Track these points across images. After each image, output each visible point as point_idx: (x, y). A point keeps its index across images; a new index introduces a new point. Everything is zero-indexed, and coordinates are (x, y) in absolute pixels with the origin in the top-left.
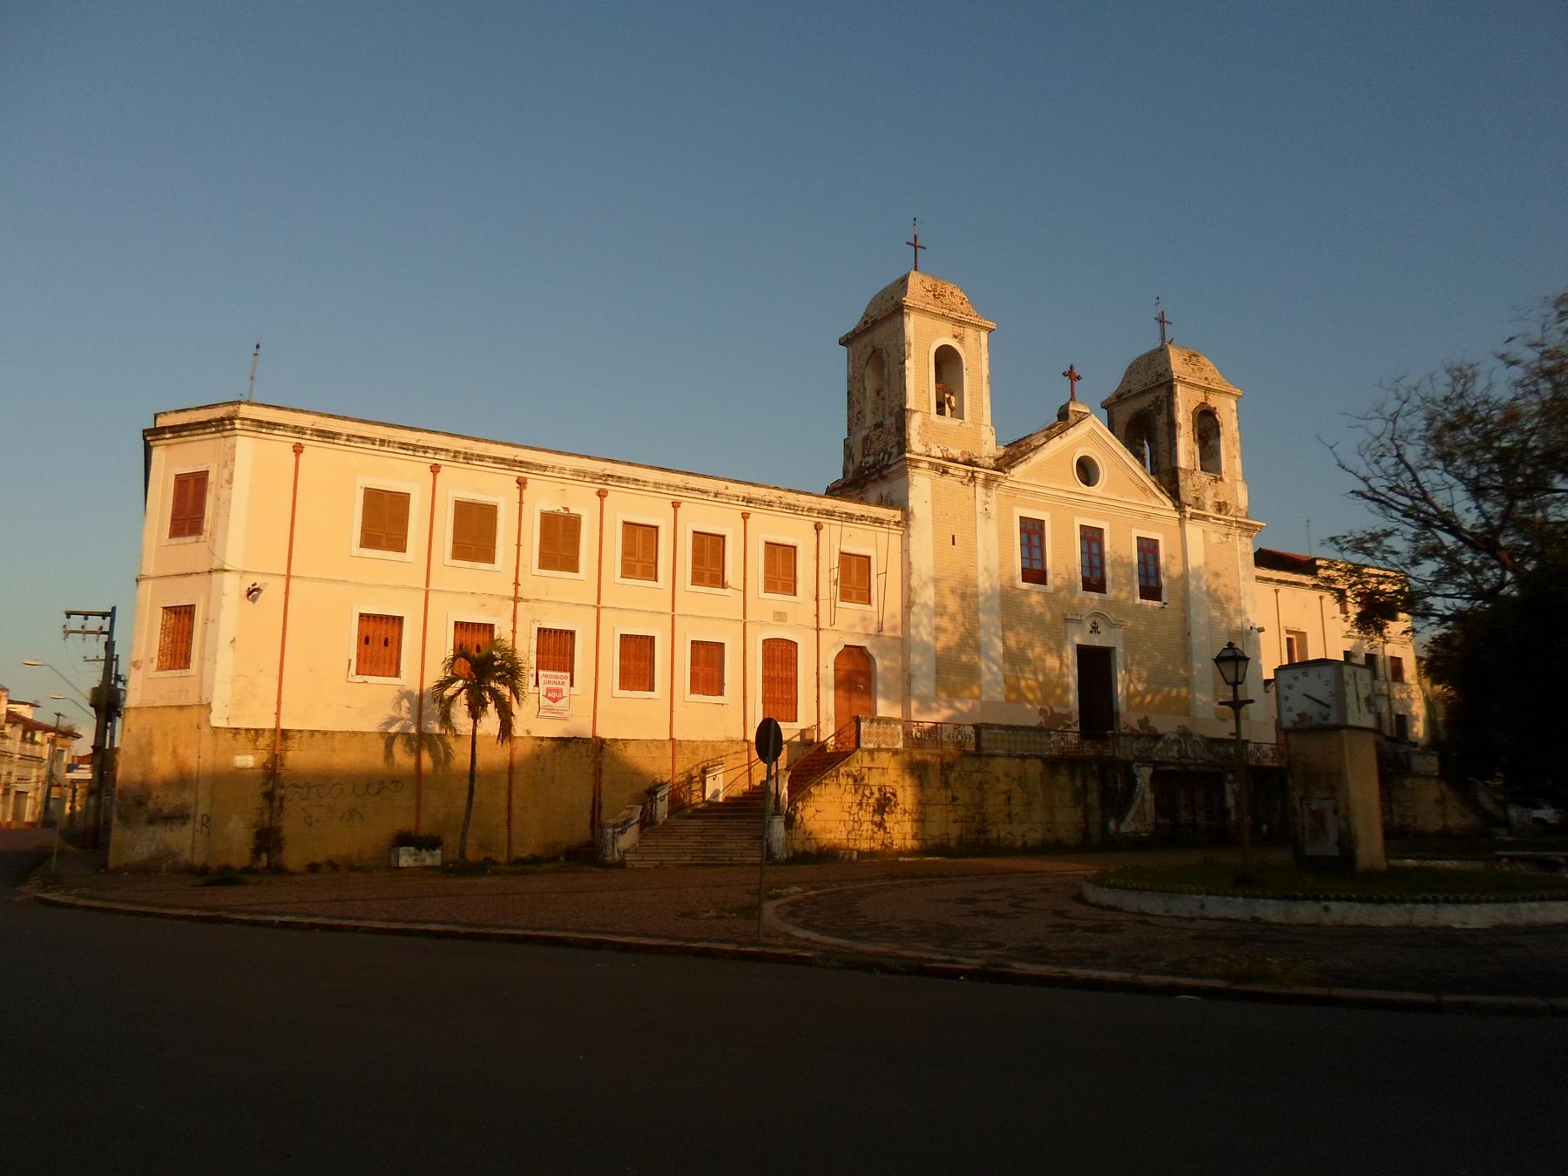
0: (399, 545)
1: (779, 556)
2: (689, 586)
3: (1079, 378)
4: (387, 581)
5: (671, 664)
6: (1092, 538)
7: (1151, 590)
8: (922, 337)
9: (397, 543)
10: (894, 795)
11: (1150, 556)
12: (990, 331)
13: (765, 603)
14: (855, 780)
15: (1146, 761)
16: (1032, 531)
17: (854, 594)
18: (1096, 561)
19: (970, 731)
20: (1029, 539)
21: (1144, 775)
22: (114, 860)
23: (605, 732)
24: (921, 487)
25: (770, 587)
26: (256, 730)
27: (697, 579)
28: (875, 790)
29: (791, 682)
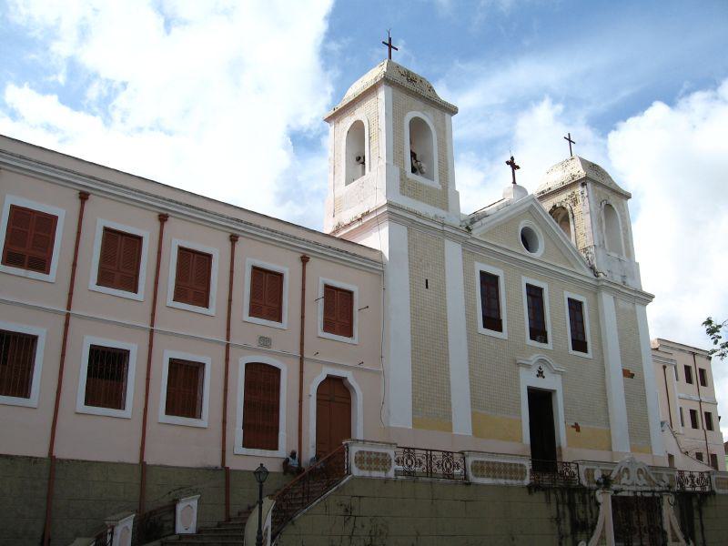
0: (42, 265)
2: (170, 302)
3: (518, 168)
5: (145, 383)
6: (535, 294)
7: (580, 344)
9: (41, 263)
13: (249, 327)
16: (489, 282)
20: (576, 325)
21: (604, 499)
22: (720, 470)
23: (60, 453)
25: (254, 311)
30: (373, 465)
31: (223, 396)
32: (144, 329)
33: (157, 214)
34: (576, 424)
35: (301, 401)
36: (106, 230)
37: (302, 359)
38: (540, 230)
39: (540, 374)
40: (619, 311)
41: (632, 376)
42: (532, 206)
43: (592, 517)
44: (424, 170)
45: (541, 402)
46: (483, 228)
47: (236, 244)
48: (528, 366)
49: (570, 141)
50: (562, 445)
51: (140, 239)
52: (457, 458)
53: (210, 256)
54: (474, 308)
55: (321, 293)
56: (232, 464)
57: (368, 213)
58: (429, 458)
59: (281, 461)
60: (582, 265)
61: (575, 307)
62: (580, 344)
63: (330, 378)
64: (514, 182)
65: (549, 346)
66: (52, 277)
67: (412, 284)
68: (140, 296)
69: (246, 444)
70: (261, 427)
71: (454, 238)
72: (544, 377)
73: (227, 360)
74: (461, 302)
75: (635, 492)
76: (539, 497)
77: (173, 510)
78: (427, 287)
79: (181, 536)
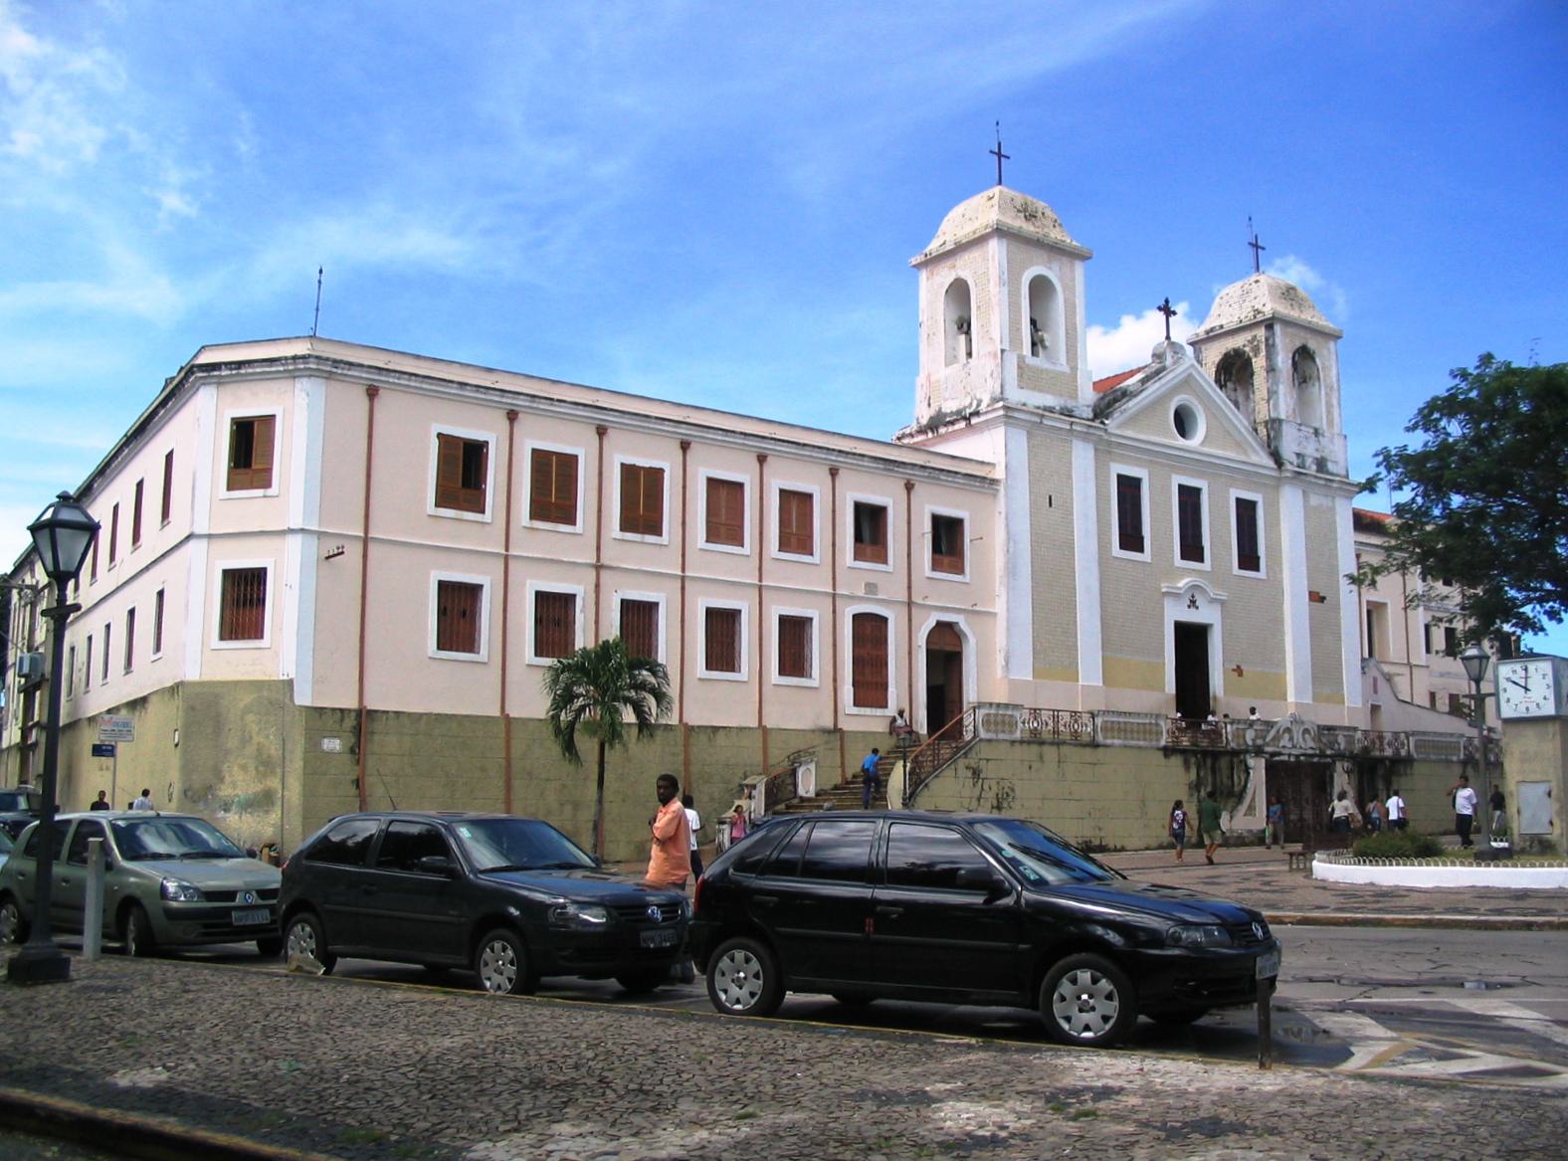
2: (928, 571)
3: (1174, 313)
4: (464, 545)
10: (1013, 790)
14: (974, 773)
15: (1258, 751)
16: (1129, 489)
19: (1066, 717)
21: (1258, 767)
26: (342, 710)
28: (993, 783)
29: (882, 663)
30: (1000, 727)
31: (831, 650)
32: (826, 593)
33: (365, 388)
34: (1238, 667)
36: (782, 491)
38: (1196, 403)
39: (1193, 603)
42: (1190, 375)
43: (1239, 784)
44: (1047, 344)
45: (1191, 641)
47: (376, 400)
50: (1217, 694)
51: (740, 486)
52: (1086, 718)
53: (810, 496)
56: (845, 725)
58: (1056, 719)
59: (888, 721)
62: (1249, 558)
64: (1168, 337)
66: (579, 528)
68: (746, 550)
69: (856, 704)
70: (870, 685)
73: (834, 612)
75: (1297, 756)
76: (1176, 761)
77: (794, 773)
78: (1050, 505)
79: (802, 799)
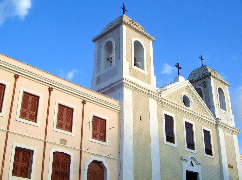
1: (21, 154)
6: (189, 127)
7: (209, 151)
8: (128, 37)
11: (208, 142)
12: (153, 41)
13: (56, 134)
16: (169, 120)
17: (64, 126)
18: (190, 138)
24: (127, 93)
27: (23, 115)
35: (80, 172)
37: (81, 151)
39: (192, 164)
40: (226, 137)
41: (232, 167)
46: (167, 94)
48: (186, 161)
49: (202, 59)
54: (162, 131)
55: (91, 119)
57: (114, 83)
60: (210, 115)
61: (207, 134)
62: (209, 151)
63: (94, 161)
65: (175, 145)
67: (134, 118)
71: (153, 97)
72: (193, 166)
74: (157, 128)
